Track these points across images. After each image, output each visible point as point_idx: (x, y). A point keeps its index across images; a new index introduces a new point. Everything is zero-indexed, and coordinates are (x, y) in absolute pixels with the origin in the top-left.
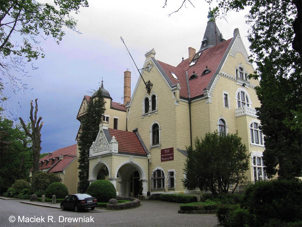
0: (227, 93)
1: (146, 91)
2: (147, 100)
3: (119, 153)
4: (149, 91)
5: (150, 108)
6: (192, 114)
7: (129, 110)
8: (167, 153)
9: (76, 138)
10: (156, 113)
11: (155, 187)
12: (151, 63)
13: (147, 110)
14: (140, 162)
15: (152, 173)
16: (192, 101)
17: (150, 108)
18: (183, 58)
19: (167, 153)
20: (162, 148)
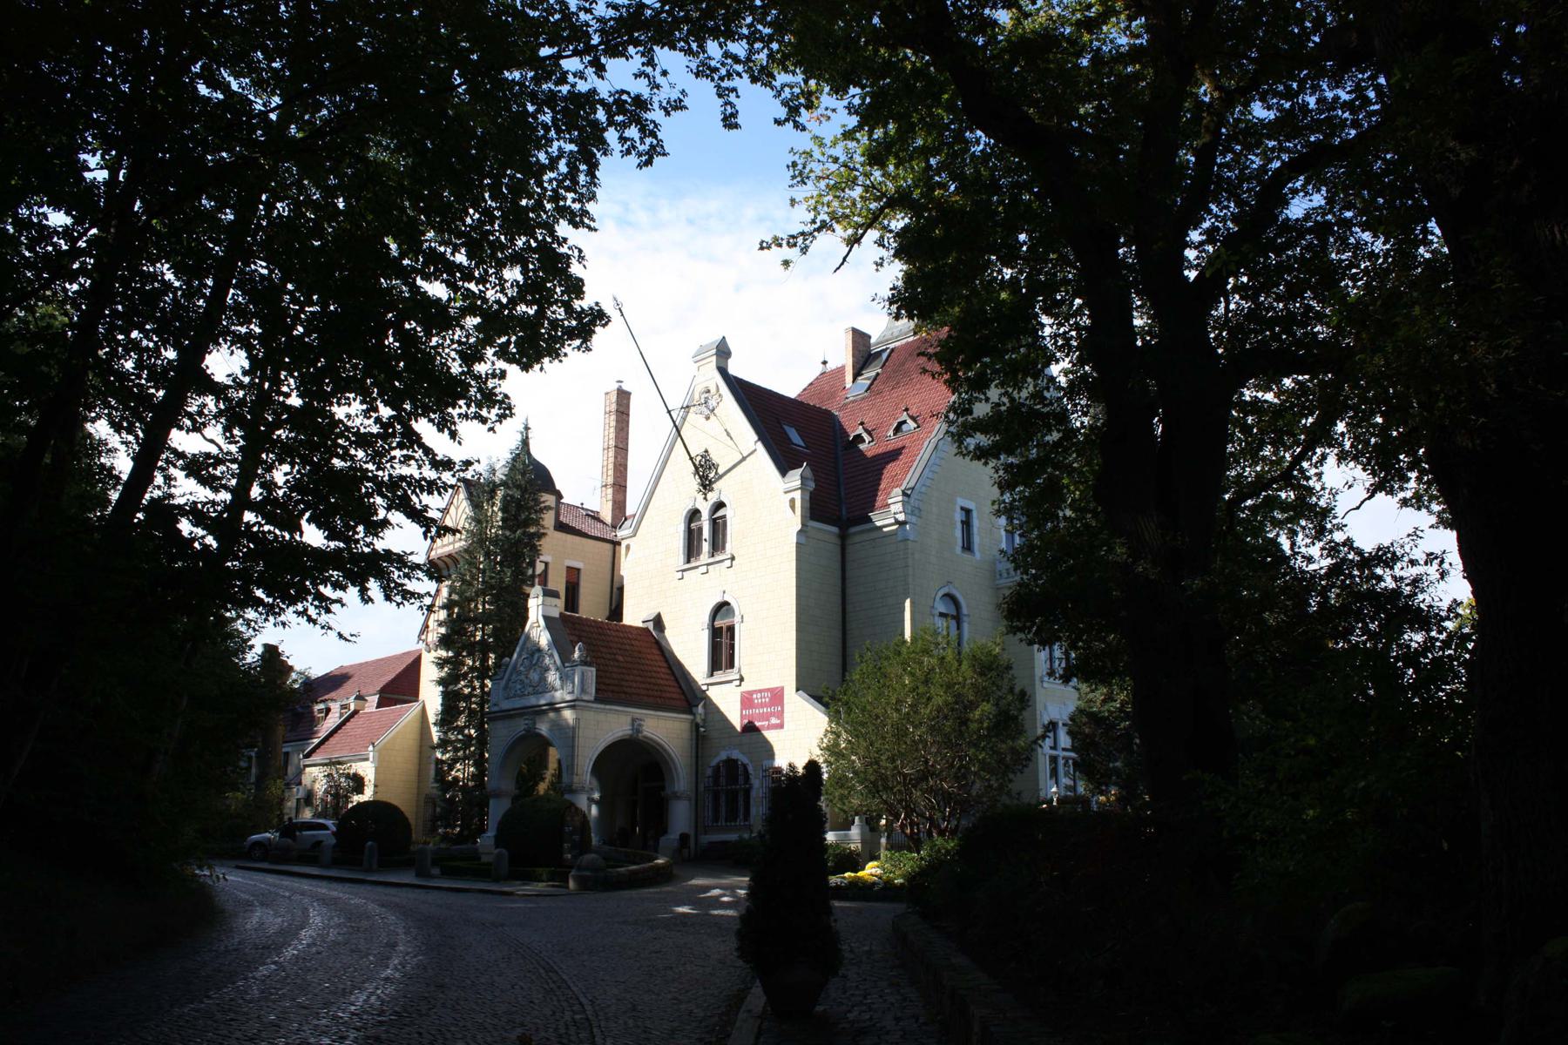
0: (970, 505)
1: (694, 483)
2: (694, 514)
3: (597, 700)
4: (706, 485)
5: (706, 547)
6: (848, 574)
7: (628, 547)
8: (762, 705)
9: (422, 632)
10: (728, 563)
11: (716, 819)
12: (713, 390)
13: (692, 550)
14: (666, 729)
15: (709, 772)
16: (853, 530)
17: (706, 547)
18: (825, 363)
19: (762, 705)
20: (746, 686)
